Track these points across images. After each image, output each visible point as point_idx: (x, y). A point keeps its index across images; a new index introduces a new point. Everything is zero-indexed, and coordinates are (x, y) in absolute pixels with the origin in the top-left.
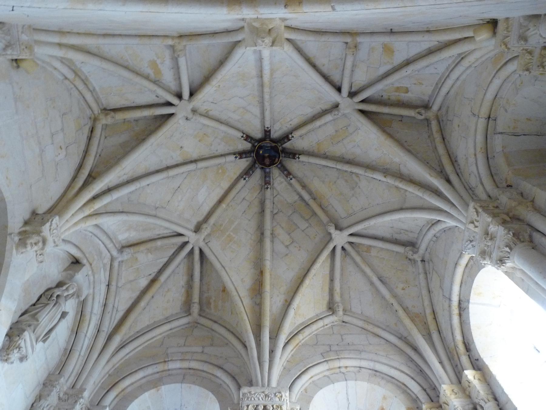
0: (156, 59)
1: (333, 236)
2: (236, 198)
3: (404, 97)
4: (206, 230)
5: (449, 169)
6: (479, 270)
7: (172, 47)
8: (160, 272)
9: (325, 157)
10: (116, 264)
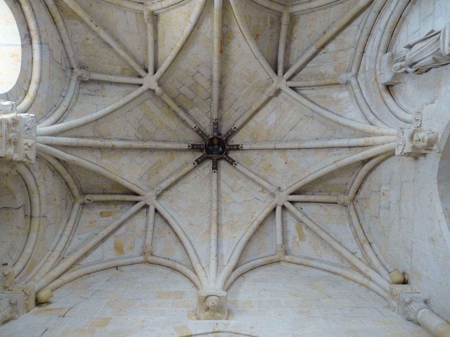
0: (300, 242)
1: (156, 84)
2: (243, 112)
3: (104, 209)
4: (271, 90)
5: (59, 167)
6: (17, 83)
7: (286, 253)
8: (315, 55)
9: (166, 150)
10: (354, 71)
